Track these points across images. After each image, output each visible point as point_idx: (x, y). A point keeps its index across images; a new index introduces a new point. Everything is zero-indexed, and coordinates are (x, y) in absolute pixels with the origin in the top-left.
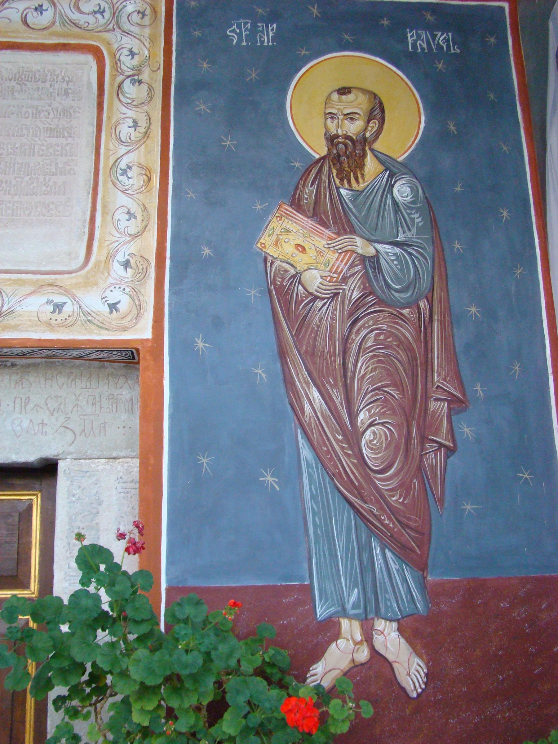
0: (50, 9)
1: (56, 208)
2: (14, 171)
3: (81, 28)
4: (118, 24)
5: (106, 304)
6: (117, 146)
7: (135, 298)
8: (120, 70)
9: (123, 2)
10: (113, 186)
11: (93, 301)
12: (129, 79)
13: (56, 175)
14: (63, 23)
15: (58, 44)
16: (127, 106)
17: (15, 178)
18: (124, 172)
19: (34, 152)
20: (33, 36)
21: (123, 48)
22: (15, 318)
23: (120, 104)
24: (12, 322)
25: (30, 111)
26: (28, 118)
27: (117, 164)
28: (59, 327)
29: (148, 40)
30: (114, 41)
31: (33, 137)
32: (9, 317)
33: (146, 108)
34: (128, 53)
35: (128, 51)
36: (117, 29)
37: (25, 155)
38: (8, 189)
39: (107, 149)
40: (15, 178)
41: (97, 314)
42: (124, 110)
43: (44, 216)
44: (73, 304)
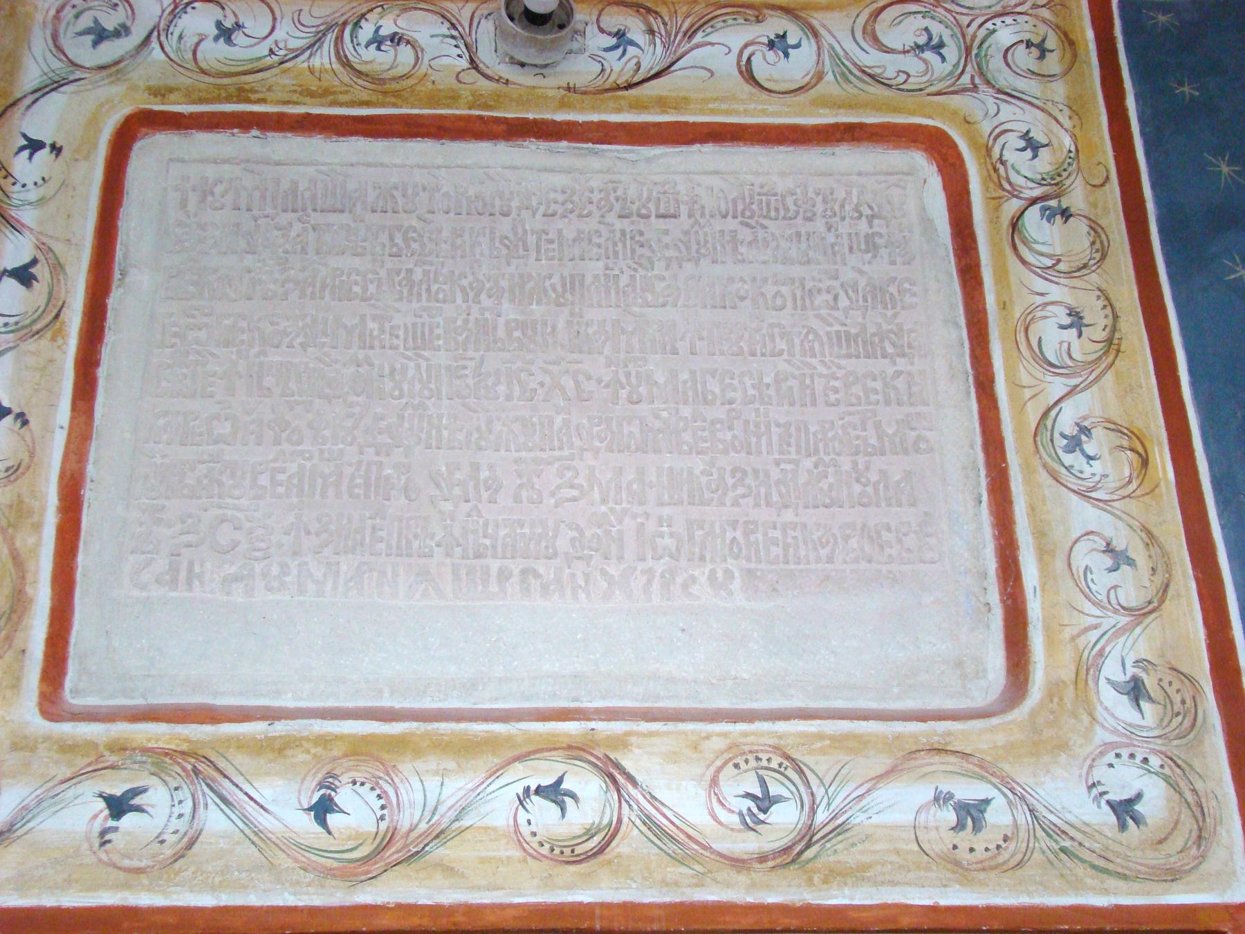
0: (804, 43)
2: (770, 444)
3: (890, 86)
5: (1103, 803)
6: (1039, 375)
7: (1182, 784)
8: (1007, 186)
10: (1050, 481)
11: (1067, 796)
12: (1037, 207)
13: (883, 454)
14: (843, 74)
15: (836, 126)
16: (1048, 272)
17: (777, 463)
18: (1074, 444)
22: (854, 845)
23: (1027, 272)
24: (850, 858)
25: (784, 290)
26: (782, 308)
27: (1049, 423)
28: (984, 870)
29: (1066, 110)
30: (978, 114)
31: (805, 355)
32: (837, 843)
33: (1094, 277)
34: (1022, 144)
35: (1021, 137)
36: (982, 87)
38: (763, 490)
39: (1015, 385)
40: (777, 463)
41: (1084, 833)
42: (1039, 284)
43: (870, 561)
44: (1010, 803)
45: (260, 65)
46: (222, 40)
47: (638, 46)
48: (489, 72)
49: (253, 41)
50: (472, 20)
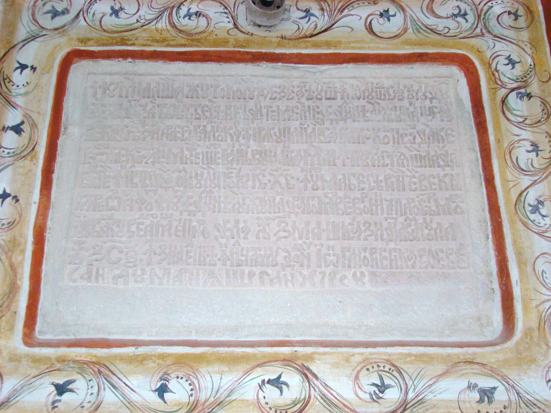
0: (398, 14)
1: (448, 258)
2: (382, 209)
3: (440, 34)
4: (486, 28)
6: (517, 176)
8: (499, 83)
9: (488, 2)
10: (524, 228)
12: (514, 93)
13: (439, 215)
14: (417, 29)
15: (414, 54)
17: (386, 220)
18: (535, 209)
19: (404, 185)
20: (381, 46)
21: (499, 56)
25: (389, 134)
29: (529, 45)
33: (544, 127)
35: (506, 59)
36: (486, 34)
37: (393, 190)
38: (379, 232)
39: (504, 180)
41: (545, 405)
42: (516, 131)
43: (433, 267)
44: (506, 389)
45: (132, 27)
46: (114, 15)
47: (316, 17)
48: (243, 30)
49: (129, 16)
50: (235, 4)
